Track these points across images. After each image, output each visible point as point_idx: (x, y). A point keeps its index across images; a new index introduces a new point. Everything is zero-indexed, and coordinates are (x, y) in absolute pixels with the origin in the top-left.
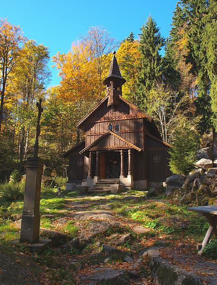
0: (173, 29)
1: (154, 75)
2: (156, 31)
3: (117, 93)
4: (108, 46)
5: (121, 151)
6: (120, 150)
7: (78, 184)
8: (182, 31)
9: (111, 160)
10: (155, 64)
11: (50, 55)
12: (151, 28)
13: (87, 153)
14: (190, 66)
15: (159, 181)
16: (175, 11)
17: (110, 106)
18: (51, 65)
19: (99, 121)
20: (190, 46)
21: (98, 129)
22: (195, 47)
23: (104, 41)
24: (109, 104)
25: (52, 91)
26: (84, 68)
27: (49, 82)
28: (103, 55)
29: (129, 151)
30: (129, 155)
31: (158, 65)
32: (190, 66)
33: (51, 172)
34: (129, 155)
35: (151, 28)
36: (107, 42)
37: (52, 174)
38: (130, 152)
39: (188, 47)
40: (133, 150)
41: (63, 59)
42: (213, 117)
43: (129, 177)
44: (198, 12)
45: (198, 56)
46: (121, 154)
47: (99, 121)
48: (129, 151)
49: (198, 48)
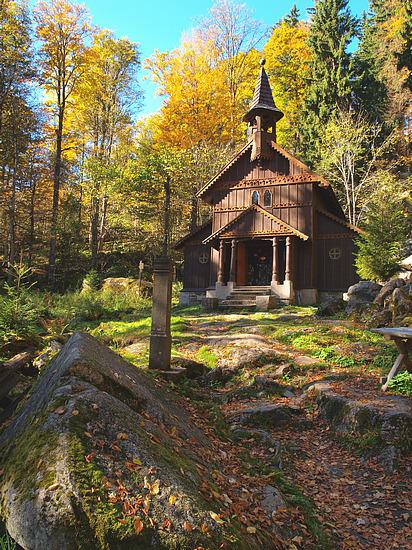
1: (335, 95)
3: (267, 139)
5: (274, 239)
6: (272, 237)
11: (142, 59)
13: (215, 243)
24: (253, 157)
26: (205, 84)
31: (343, 74)
40: (295, 239)
43: (287, 283)
46: (274, 244)
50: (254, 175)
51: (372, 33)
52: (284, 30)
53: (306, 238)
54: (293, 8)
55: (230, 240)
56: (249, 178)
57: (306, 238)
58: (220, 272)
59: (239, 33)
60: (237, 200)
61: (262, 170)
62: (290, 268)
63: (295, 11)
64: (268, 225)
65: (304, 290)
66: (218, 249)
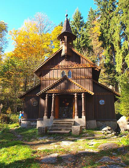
0: (88, 21)
1: (80, 46)
2: (81, 18)
3: (70, 47)
4: (48, 26)
5: (76, 94)
6: (75, 93)
7: (32, 122)
8: (95, 22)
9: (63, 102)
10: (81, 39)
11: (8, 30)
12: (78, 16)
13: (43, 96)
14: (100, 43)
15: (105, 121)
16: (90, 11)
17: (64, 56)
18: (8, 36)
19: (53, 68)
20: (101, 30)
21: (52, 75)
22: (105, 30)
23: (44, 24)
24: (63, 53)
25: (8, 55)
26: (32, 38)
27: (6, 47)
28: (44, 32)
29: (83, 94)
30: (83, 99)
31: (82, 40)
32: (100, 43)
33: (7, 109)
34: (83, 99)
35: (78, 16)
36: (47, 23)
37: (8, 112)
38: (84, 95)
39: (100, 31)
40: (87, 94)
41: (16, 33)
42: (117, 76)
43: (84, 117)
44: (107, 9)
45: (107, 36)
46: (76, 97)
47: (53, 68)
48: (83, 94)
49: (107, 32)
50: (63, 63)
51: (87, 32)
52: (59, 27)
53: (93, 94)
54: (61, 22)
55: (52, 94)
56: (60, 64)
57: (93, 94)
58: (46, 111)
59: (44, 24)
60: (55, 75)
61: (67, 61)
62: (84, 109)
63: (62, 23)
64: (77, 87)
65: (91, 121)
66: (44, 99)
